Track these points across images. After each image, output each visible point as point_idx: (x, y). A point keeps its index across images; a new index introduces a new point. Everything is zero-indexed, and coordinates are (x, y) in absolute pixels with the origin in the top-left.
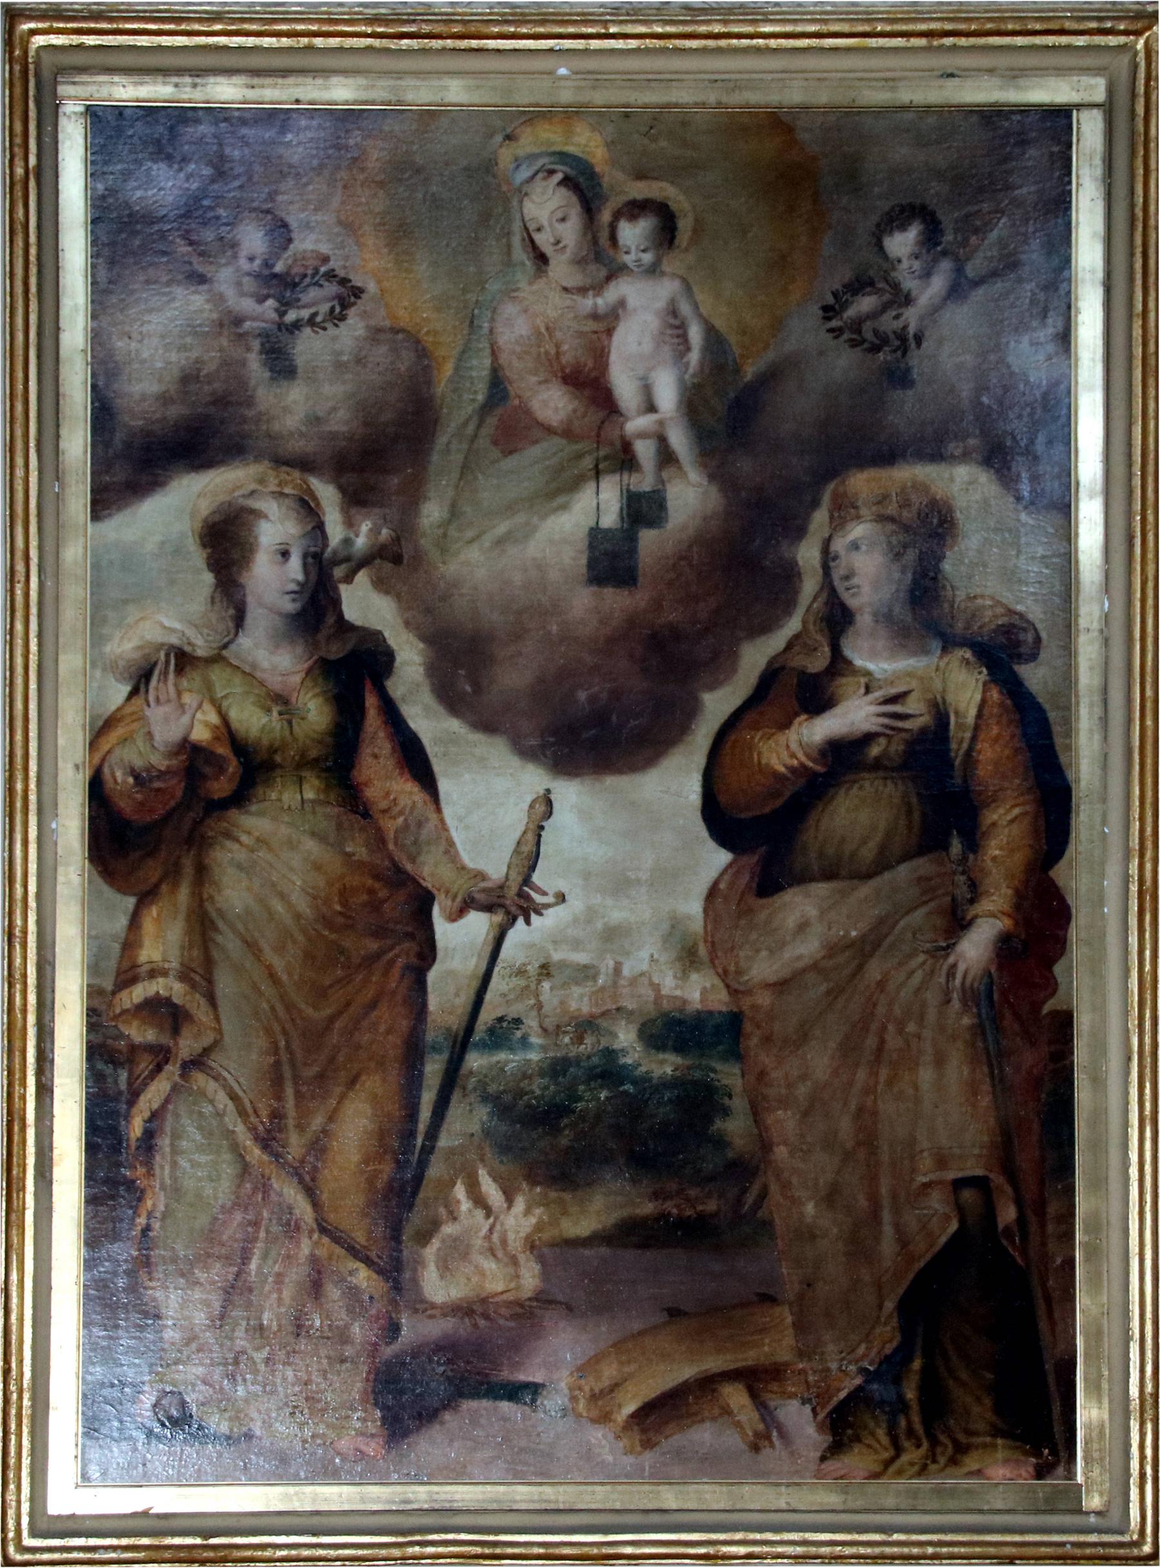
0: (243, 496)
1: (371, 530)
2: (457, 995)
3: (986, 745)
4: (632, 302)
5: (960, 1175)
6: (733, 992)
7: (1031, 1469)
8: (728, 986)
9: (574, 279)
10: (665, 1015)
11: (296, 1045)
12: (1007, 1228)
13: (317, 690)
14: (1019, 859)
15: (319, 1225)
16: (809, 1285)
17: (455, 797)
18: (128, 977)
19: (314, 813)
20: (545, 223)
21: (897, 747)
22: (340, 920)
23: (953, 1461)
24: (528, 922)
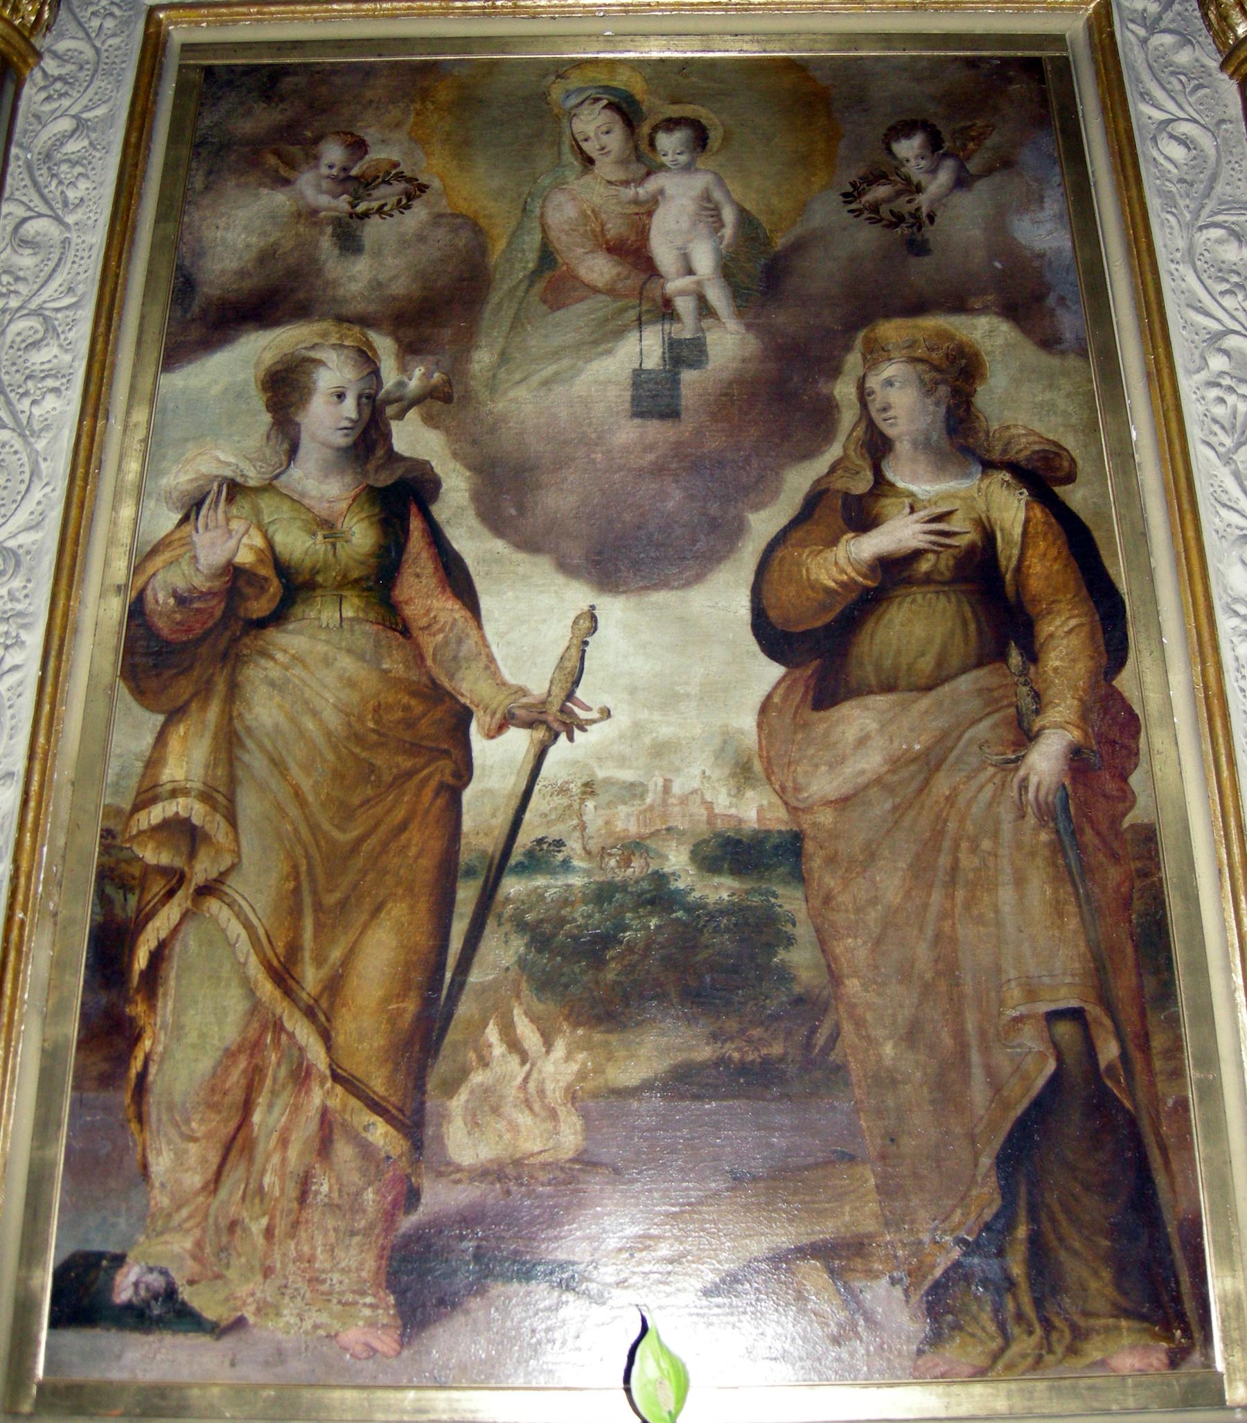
0: (306, 348)
1: (424, 374)
2: (494, 815)
3: (1035, 560)
4: (669, 191)
5: (1053, 1007)
6: (793, 810)
7: (1163, 1357)
8: (786, 803)
9: (618, 174)
10: (717, 835)
11: (319, 871)
12: (1110, 1068)
13: (363, 515)
14: (1082, 668)
15: (333, 1072)
16: (892, 1140)
17: (496, 614)
19: (352, 631)
20: (592, 134)
21: (946, 562)
22: (374, 737)
23: (1072, 1351)
24: (571, 739)
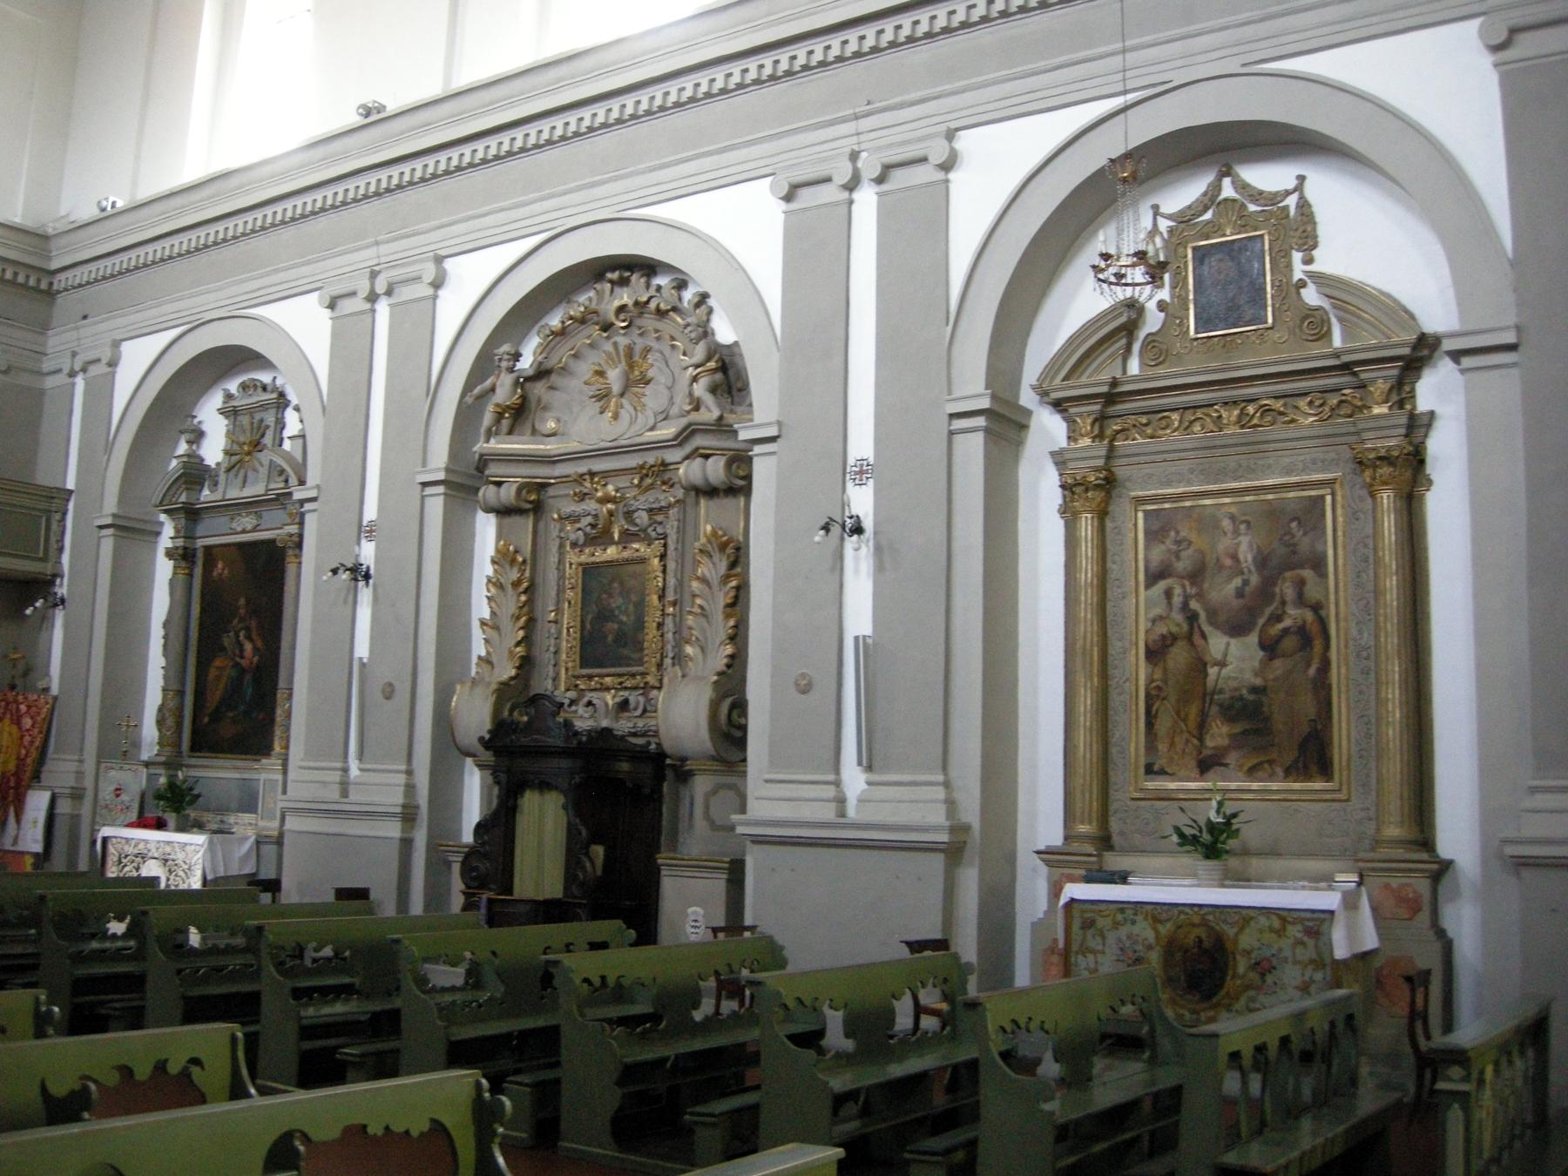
18: (1153, 681)
